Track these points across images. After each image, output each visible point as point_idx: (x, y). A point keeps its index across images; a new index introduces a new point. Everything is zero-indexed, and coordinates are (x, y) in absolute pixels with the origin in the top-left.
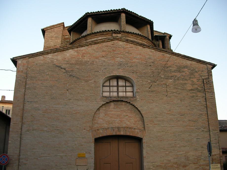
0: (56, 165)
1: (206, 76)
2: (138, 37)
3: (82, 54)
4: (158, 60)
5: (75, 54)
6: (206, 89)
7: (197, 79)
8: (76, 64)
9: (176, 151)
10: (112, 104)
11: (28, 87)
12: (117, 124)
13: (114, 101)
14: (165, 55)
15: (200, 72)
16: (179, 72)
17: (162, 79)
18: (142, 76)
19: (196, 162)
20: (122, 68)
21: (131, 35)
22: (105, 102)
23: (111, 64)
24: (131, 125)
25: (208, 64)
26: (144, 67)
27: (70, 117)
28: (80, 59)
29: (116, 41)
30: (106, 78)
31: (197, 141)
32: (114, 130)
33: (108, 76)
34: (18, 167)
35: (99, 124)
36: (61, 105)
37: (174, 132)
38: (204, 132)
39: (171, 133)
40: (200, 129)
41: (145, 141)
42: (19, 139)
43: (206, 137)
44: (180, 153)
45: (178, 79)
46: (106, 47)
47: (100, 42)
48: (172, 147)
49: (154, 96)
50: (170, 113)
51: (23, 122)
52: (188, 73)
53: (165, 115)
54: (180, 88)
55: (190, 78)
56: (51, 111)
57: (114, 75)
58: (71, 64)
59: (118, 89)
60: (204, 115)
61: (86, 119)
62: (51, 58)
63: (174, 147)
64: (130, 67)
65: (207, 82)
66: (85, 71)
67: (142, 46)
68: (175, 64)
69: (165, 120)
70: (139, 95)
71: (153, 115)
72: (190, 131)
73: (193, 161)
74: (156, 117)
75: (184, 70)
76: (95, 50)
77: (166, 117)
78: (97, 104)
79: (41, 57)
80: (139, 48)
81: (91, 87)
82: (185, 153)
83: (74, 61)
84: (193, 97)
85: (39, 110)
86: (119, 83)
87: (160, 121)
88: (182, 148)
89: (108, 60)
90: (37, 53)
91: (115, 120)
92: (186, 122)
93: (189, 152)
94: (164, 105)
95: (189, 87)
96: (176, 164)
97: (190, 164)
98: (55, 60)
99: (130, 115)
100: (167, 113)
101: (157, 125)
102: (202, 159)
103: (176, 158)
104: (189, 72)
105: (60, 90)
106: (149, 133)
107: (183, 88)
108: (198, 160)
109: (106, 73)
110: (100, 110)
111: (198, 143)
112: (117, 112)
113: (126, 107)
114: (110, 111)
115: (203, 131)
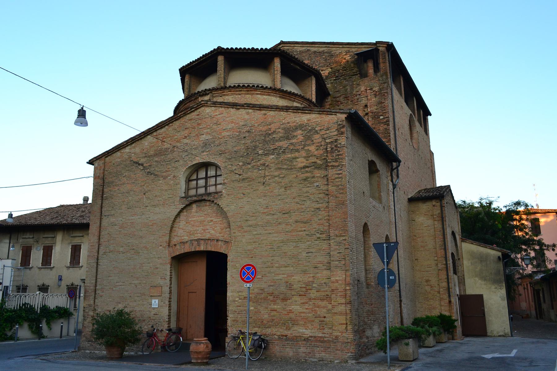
2: (241, 91)
3: (161, 138)
5: (154, 140)
8: (155, 156)
9: (273, 273)
10: (194, 206)
11: (106, 197)
12: (199, 235)
15: (323, 132)
16: (288, 138)
17: (260, 157)
20: (207, 150)
25: (338, 113)
27: (147, 230)
28: (160, 147)
32: (192, 244)
35: (179, 236)
36: (137, 216)
37: (271, 243)
39: (266, 244)
42: (95, 266)
44: (279, 278)
47: (181, 116)
50: (266, 212)
51: (100, 243)
55: (305, 145)
57: (197, 162)
59: (206, 183)
63: (270, 267)
65: (332, 149)
67: (235, 107)
71: (243, 217)
73: (299, 291)
74: (247, 221)
75: (295, 134)
76: (176, 129)
77: (261, 218)
78: (176, 208)
79: (118, 154)
82: (286, 278)
83: (153, 151)
84: (305, 180)
85: (116, 225)
87: (251, 226)
90: (113, 148)
93: (293, 276)
94: (259, 200)
95: (301, 162)
96: (272, 296)
97: (294, 296)
98: (133, 155)
99: (215, 220)
102: (313, 288)
104: (304, 135)
105: (136, 196)
106: (236, 246)
108: (307, 289)
112: (200, 217)
113: (210, 208)
114: (192, 216)
115: (319, 238)
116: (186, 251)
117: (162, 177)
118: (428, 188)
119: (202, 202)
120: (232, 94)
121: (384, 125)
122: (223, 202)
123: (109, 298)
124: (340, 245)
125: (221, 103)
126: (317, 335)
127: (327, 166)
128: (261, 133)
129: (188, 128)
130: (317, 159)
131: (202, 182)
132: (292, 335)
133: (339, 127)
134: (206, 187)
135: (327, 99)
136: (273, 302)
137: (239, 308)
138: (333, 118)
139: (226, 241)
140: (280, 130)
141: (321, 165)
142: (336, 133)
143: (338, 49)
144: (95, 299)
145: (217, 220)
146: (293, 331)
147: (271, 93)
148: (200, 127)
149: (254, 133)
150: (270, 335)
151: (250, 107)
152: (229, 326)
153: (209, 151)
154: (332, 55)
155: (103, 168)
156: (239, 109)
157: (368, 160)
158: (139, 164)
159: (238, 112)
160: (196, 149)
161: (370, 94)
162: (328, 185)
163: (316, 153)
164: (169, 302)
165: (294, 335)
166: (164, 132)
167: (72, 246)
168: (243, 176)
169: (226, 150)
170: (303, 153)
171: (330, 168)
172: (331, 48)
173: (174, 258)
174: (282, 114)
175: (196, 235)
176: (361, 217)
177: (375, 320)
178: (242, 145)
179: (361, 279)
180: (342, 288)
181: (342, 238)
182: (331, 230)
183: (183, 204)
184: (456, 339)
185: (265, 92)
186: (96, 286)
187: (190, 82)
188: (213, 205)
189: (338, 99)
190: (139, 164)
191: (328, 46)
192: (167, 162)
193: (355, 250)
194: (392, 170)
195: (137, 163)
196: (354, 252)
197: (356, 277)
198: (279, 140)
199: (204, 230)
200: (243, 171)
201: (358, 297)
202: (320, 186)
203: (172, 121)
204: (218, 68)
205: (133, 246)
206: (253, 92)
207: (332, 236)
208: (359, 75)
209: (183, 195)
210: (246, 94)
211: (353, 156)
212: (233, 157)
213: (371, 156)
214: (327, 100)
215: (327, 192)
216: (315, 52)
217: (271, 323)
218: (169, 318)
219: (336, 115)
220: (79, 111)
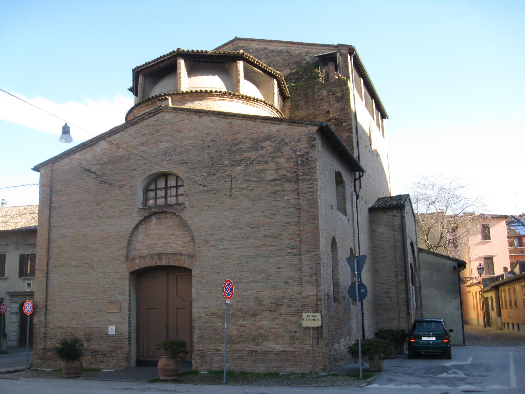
0: (86, 313)
1: (305, 148)
4: (221, 134)
6: (301, 176)
7: (287, 159)
9: (242, 289)
10: (154, 218)
12: (160, 248)
13: (155, 214)
16: (256, 149)
17: (225, 168)
18: (195, 168)
20: (168, 159)
22: (143, 216)
23: (152, 155)
26: (198, 151)
27: (101, 243)
31: (277, 272)
33: (148, 174)
34: (44, 316)
38: (291, 255)
40: (285, 251)
41: (194, 273)
42: (45, 280)
43: (295, 265)
45: (252, 164)
46: (147, 128)
52: (270, 149)
53: (226, 230)
54: (253, 179)
55: (274, 157)
58: (102, 164)
59: (166, 193)
60: (293, 224)
65: (303, 162)
66: (119, 172)
68: (250, 136)
69: (226, 238)
70: (188, 200)
72: (267, 255)
74: (212, 234)
77: (228, 232)
79: (67, 160)
80: (193, 118)
81: (126, 195)
82: (256, 293)
84: (275, 193)
85: (66, 237)
86: (178, 183)
88: (251, 284)
89: (149, 149)
91: (158, 242)
93: (263, 292)
94: (226, 213)
95: (270, 175)
96: (240, 312)
99: (177, 234)
100: (230, 227)
101: (212, 246)
102: (284, 304)
103: (241, 302)
104: (273, 146)
107: (259, 179)
108: (278, 305)
109: (146, 171)
111: (280, 275)
114: (151, 229)
115: (290, 253)
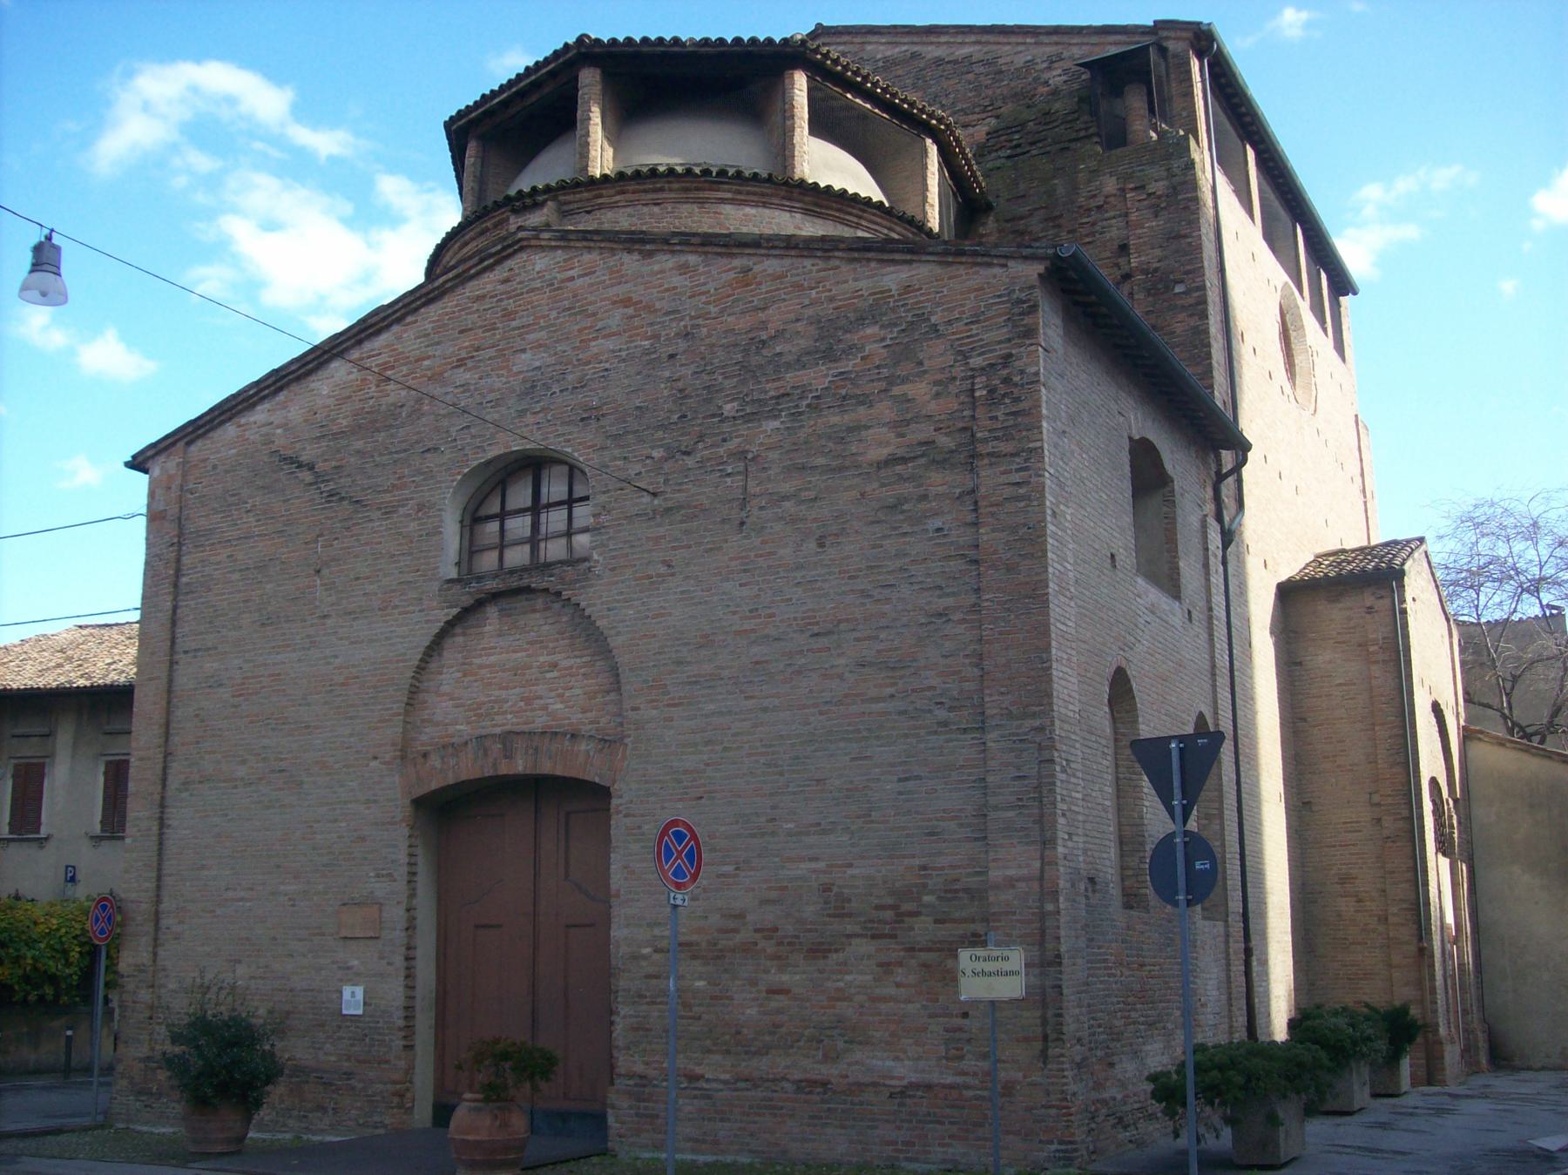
2: (661, 190)
6: (985, 441)
10: (492, 612)
11: (187, 584)
12: (509, 716)
14: (757, 268)
16: (829, 356)
17: (726, 427)
18: (627, 433)
19: (887, 929)
20: (538, 407)
21: (612, 192)
24: (569, 719)
27: (326, 703)
29: (519, 256)
30: (465, 475)
32: (486, 751)
36: (294, 651)
42: (155, 829)
43: (962, 767)
48: (753, 836)
49: (676, 540)
55: (891, 381)
56: (260, 682)
60: (957, 616)
61: (380, 707)
62: (264, 425)
64: (572, 393)
65: (992, 391)
74: (679, 663)
79: (230, 430)
82: (825, 872)
85: (221, 685)
87: (696, 682)
90: (211, 410)
92: (841, 677)
95: (878, 444)
96: (771, 938)
97: (854, 941)
98: (279, 431)
100: (737, 633)
104: (888, 342)
110: (445, 653)
113: (550, 621)
114: (484, 649)
115: (945, 724)
116: (464, 777)
117: (380, 509)
118: (1347, 548)
119: (520, 597)
120: (631, 204)
121: (1191, 316)
122: (595, 598)
123: (203, 945)
124: (1022, 751)
125: (589, 236)
126: (936, 1081)
127: (974, 456)
128: (732, 339)
129: (471, 329)
130: (935, 430)
131: (519, 526)
132: (846, 1081)
133: (1016, 310)
134: (534, 540)
135: (984, 224)
136: (775, 962)
137: (654, 982)
138: (995, 277)
139: (606, 741)
140: (799, 326)
141: (952, 452)
142: (1003, 333)
143: (1020, 48)
144: (155, 946)
145: (573, 661)
146: (849, 1064)
147: (772, 195)
148: (514, 324)
149: (707, 341)
150: (768, 1080)
151: (692, 244)
152: (617, 1047)
153: (543, 409)
154: (1001, 72)
155: (179, 481)
156: (650, 254)
157: (1131, 439)
158: (300, 466)
159: (649, 264)
160: (497, 403)
161: (1137, 204)
162: (975, 524)
163: (932, 407)
164: (408, 959)
165: (851, 1080)
166: (387, 346)
167: (108, 764)
168: (666, 499)
169: (605, 404)
170: (885, 410)
171: (986, 461)
172: (994, 47)
173: (419, 803)
174: (809, 267)
175: (499, 719)
176: (1104, 644)
177: (1154, 1023)
178: (663, 386)
179: (1101, 874)
180: (1030, 908)
181: (1029, 723)
182: (991, 695)
183: (451, 607)
184: (1443, 1083)
185: (748, 193)
186: (158, 899)
187: (482, 166)
188: (557, 606)
189: (1021, 224)
190: (300, 466)
191: (985, 38)
192: (396, 452)
193: (1079, 767)
194: (1220, 477)
195: (291, 460)
196: (1074, 776)
197: (1082, 865)
198: (799, 364)
199: (528, 701)
200: (666, 481)
201: (1091, 940)
202: (950, 529)
203: (414, 306)
204: (579, 113)
205: (281, 760)
206: (707, 194)
207: (992, 716)
208: (1096, 139)
209: (453, 574)
210: (677, 202)
211: (1072, 419)
212: (629, 429)
213: (1139, 421)
214: (982, 230)
215: (971, 553)
216: (939, 62)
217: (767, 1038)
218: (406, 1017)
219: (1005, 266)
220: (38, 249)
